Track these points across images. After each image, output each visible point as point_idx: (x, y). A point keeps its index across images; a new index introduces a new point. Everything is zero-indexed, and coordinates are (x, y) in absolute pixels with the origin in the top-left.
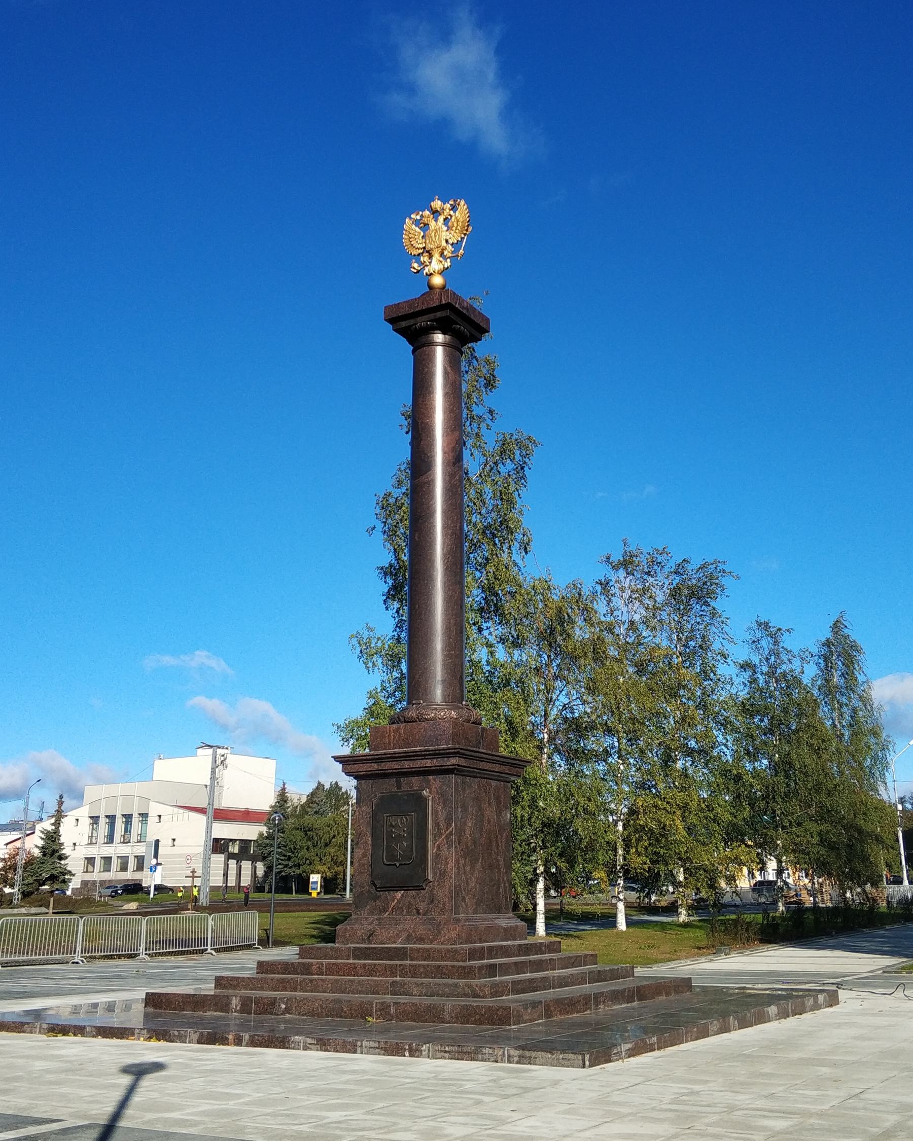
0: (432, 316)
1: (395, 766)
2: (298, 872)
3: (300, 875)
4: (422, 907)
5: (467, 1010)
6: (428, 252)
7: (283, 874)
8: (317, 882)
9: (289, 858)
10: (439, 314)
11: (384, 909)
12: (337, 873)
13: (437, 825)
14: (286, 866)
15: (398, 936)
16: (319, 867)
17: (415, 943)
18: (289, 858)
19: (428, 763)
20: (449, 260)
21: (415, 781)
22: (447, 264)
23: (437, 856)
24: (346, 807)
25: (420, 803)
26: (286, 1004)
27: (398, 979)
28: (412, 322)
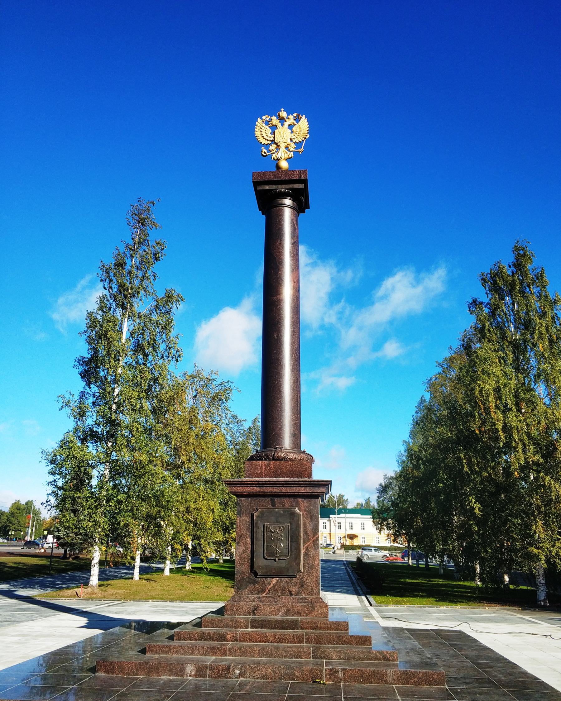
0: (291, 186)
1: (275, 490)
4: (294, 589)
5: (407, 674)
6: (276, 144)
10: (296, 186)
13: (305, 532)
15: (279, 610)
17: (293, 616)
19: (302, 490)
20: (292, 153)
21: (286, 501)
22: (291, 155)
23: (306, 555)
26: (241, 669)
27: (305, 644)
28: (274, 187)
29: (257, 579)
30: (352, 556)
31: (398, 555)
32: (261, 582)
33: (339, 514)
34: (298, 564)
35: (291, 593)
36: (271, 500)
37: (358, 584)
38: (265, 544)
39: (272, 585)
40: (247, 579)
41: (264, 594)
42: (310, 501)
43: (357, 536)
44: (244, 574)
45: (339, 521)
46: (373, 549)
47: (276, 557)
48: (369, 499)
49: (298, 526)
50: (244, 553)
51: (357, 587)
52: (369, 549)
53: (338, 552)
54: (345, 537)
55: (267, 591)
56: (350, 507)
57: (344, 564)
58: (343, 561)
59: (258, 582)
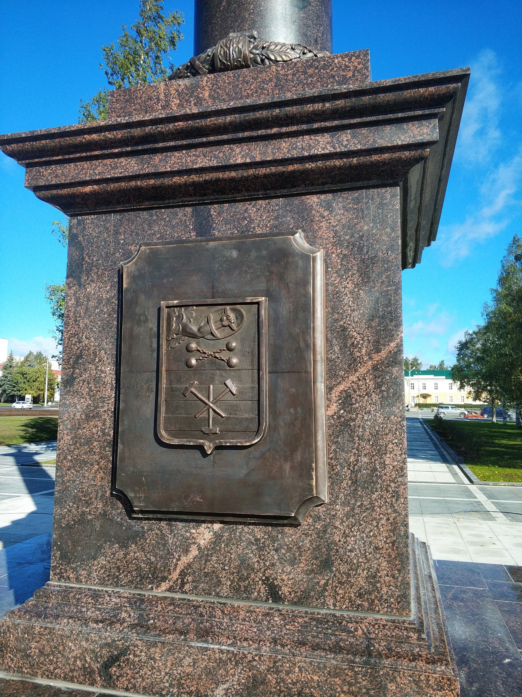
2: (19, 393)
3: (20, 395)
4: (290, 578)
7: (11, 394)
8: (29, 399)
9: (14, 387)
11: (154, 571)
12: (39, 395)
14: (13, 390)
16: (30, 392)
18: (14, 387)
21: (259, 215)
23: (342, 427)
24: (45, 364)
25: (282, 267)
29: (136, 526)
30: (429, 414)
31: (477, 412)
32: (151, 538)
33: (412, 375)
34: (306, 469)
35: (274, 594)
36: (195, 214)
37: (443, 447)
38: (164, 384)
39: (194, 552)
40: (98, 525)
41: (164, 586)
42: (357, 201)
43: (430, 396)
44: (88, 504)
45: (412, 383)
46: (450, 407)
47: (205, 435)
48: (443, 361)
49: (304, 308)
50: (88, 418)
51: (442, 450)
52: (445, 407)
53: (412, 410)
54: (418, 396)
55: (175, 575)
56: (423, 368)
57: (421, 422)
58: (418, 419)
59: (142, 535)
